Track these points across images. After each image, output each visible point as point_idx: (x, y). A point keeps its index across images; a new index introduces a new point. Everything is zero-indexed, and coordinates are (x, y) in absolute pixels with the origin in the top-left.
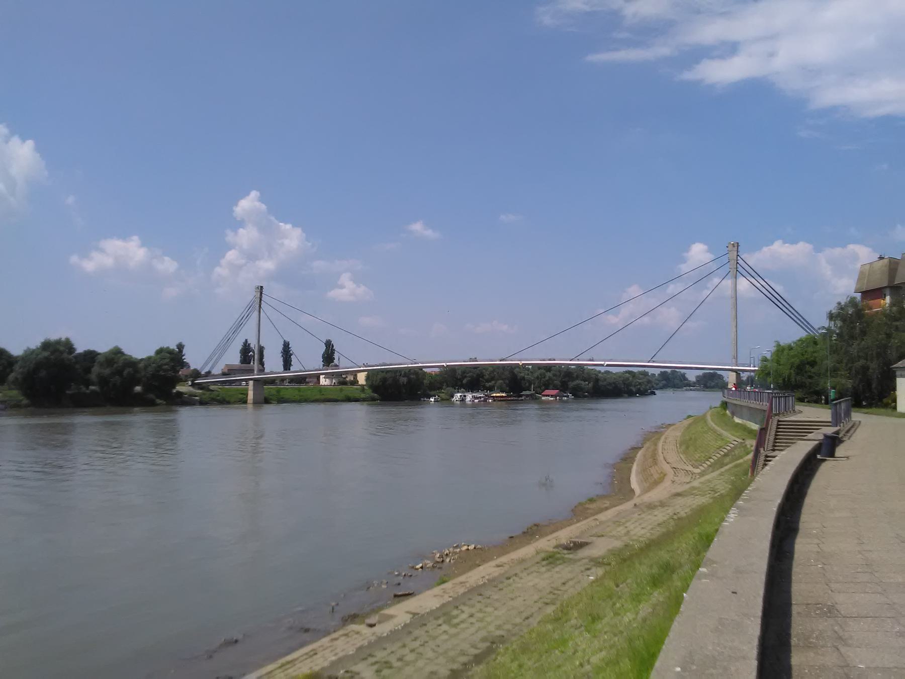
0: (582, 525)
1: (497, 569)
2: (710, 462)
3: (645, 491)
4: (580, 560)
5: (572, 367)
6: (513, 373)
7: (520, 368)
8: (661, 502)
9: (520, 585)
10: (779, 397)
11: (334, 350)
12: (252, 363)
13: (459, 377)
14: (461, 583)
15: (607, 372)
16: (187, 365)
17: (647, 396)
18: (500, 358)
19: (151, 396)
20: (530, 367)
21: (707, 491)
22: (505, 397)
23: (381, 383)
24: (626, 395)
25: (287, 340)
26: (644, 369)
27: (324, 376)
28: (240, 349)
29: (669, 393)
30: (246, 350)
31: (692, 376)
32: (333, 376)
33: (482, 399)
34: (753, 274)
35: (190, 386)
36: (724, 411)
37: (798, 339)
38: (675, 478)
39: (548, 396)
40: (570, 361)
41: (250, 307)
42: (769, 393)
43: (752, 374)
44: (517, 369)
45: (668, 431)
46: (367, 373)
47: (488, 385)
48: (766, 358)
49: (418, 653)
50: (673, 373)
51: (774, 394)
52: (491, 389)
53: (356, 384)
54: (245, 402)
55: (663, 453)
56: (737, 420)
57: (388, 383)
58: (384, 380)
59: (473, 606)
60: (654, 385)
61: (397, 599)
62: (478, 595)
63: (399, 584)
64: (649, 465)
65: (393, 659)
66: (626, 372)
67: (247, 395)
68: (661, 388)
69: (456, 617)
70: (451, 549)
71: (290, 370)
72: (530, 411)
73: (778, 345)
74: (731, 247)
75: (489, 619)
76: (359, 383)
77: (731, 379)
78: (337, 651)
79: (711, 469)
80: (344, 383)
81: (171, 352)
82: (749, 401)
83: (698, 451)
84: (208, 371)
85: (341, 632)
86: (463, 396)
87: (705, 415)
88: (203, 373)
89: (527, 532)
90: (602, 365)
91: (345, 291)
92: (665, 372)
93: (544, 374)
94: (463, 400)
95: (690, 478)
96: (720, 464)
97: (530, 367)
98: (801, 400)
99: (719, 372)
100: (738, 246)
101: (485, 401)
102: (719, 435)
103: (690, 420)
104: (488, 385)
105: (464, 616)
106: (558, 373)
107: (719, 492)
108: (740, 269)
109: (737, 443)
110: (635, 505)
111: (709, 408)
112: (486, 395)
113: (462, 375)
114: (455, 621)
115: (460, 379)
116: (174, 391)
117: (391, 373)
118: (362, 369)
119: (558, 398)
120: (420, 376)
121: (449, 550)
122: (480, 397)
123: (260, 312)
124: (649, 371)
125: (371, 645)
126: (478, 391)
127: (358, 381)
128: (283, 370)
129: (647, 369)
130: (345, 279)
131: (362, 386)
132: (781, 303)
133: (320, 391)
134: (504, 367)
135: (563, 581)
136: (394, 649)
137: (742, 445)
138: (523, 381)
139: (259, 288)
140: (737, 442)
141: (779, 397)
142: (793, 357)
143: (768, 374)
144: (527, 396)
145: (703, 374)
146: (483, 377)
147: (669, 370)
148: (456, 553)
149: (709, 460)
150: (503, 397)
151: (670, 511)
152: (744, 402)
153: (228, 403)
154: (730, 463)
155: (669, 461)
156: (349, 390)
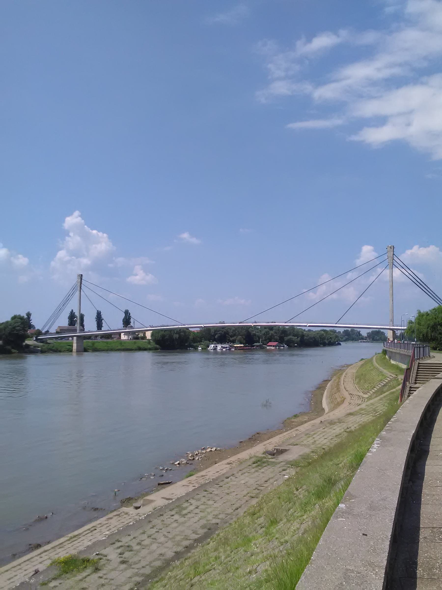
0: (286, 435)
1: (228, 466)
2: (372, 392)
3: (331, 410)
4: (279, 463)
5: (287, 327)
6: (248, 332)
7: (253, 328)
8: (339, 419)
9: (235, 483)
10: (419, 347)
11: (130, 316)
12: (76, 325)
13: (212, 334)
14: (202, 476)
15: (309, 331)
16: (33, 327)
17: (335, 346)
18: (240, 322)
19: (9, 347)
20: (259, 327)
21: (370, 411)
22: (243, 347)
23: (161, 338)
24: (322, 345)
25: (100, 310)
26: (334, 328)
27: (123, 334)
28: (68, 316)
29: (350, 344)
30: (72, 316)
31: (364, 333)
32: (130, 333)
33: (228, 348)
34: (405, 267)
35: (34, 340)
36: (384, 356)
37: (433, 308)
38: (351, 401)
39: (271, 346)
40: (285, 323)
41: (74, 288)
42: (413, 344)
43: (403, 331)
44: (251, 329)
45: (348, 370)
46: (152, 331)
47: (231, 339)
48: (412, 321)
49: (153, 539)
50: (352, 331)
51: (416, 345)
52: (234, 342)
53: (146, 339)
54: (71, 351)
55: (344, 384)
56: (393, 362)
57: (166, 338)
58: (163, 336)
59: (199, 500)
60: (340, 339)
61: (160, 486)
62: (204, 491)
63: (163, 476)
64: (335, 392)
65: (133, 544)
66: (322, 330)
67: (72, 346)
68: (345, 341)
69: (185, 508)
70: (200, 451)
71: (101, 329)
72: (259, 356)
73: (420, 312)
74: (389, 249)
75: (209, 510)
76: (147, 338)
77: (389, 335)
78: (111, 527)
79: (375, 395)
80: (137, 338)
81: (21, 318)
82: (400, 350)
83: (367, 382)
84: (46, 330)
85: (115, 513)
86: (215, 347)
87: (372, 359)
88: (43, 332)
89: (252, 438)
90: (306, 326)
91: (138, 277)
92: (347, 330)
93: (268, 332)
94: (215, 349)
95: (361, 401)
96: (381, 391)
97: (259, 327)
98: (435, 349)
99: (382, 330)
100: (394, 248)
101: (230, 350)
102: (381, 372)
103: (362, 362)
104: (231, 339)
105: (191, 508)
106: (277, 331)
107: (379, 412)
108: (395, 263)
109: (392, 377)
110: (321, 422)
111: (375, 354)
112: (230, 346)
113: (214, 333)
114: (184, 512)
115: (213, 335)
116: (24, 344)
117: (167, 331)
118: (148, 329)
119: (277, 347)
120: (187, 334)
121: (198, 452)
122: (227, 347)
123: (80, 291)
124: (337, 330)
125: (119, 532)
126: (225, 343)
127: (146, 337)
128: (97, 329)
129: (335, 329)
130: (138, 269)
131: (149, 340)
132: (422, 285)
133: (121, 343)
134: (242, 327)
135: (266, 479)
136: (135, 535)
137: (396, 379)
138: (254, 337)
139: (80, 276)
140: (393, 377)
141: (419, 347)
142: (429, 320)
143: (413, 332)
144: (257, 346)
145: (371, 332)
146: (228, 334)
147: (350, 329)
148: (203, 453)
149: (374, 388)
150: (241, 347)
151: (345, 426)
152: (397, 350)
153: (60, 351)
154: (387, 391)
155: (348, 389)
156: (140, 343)
